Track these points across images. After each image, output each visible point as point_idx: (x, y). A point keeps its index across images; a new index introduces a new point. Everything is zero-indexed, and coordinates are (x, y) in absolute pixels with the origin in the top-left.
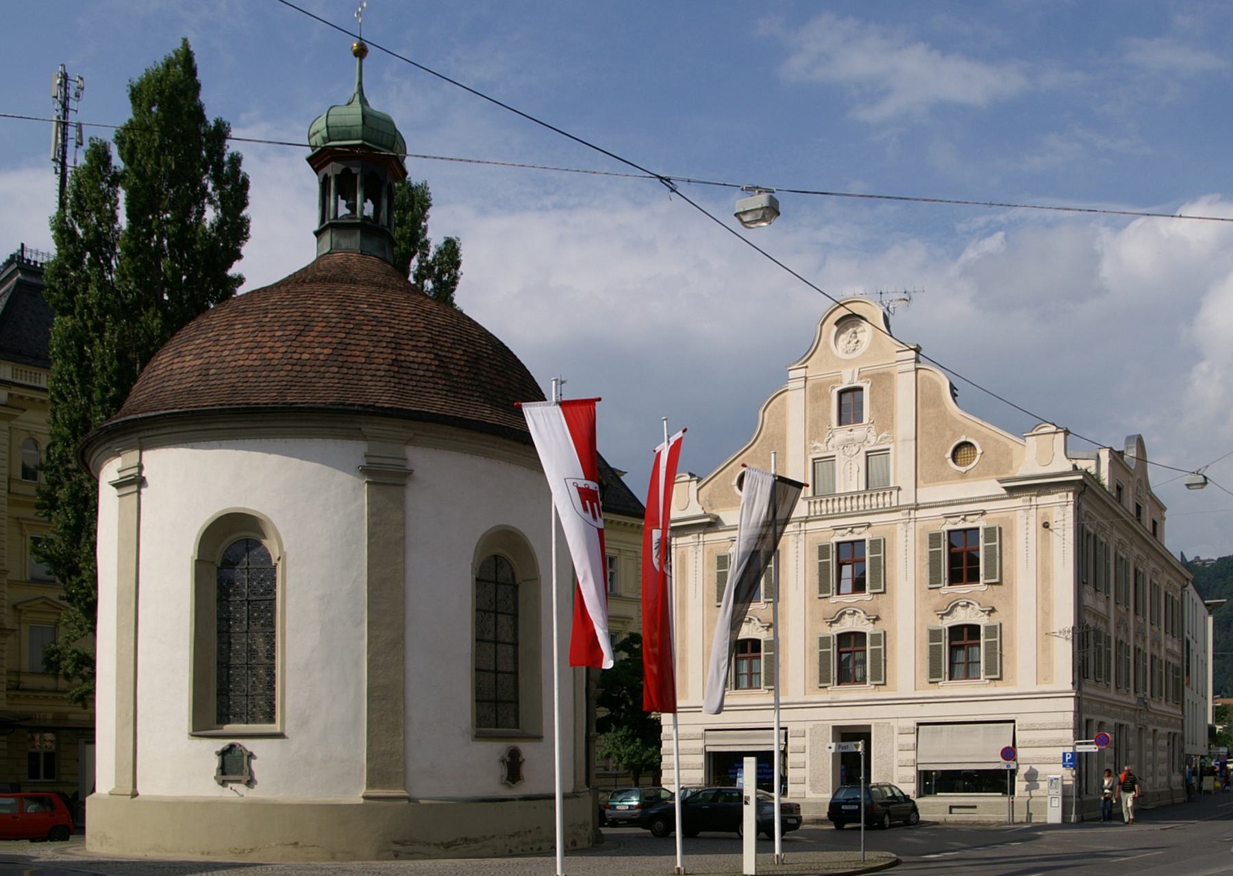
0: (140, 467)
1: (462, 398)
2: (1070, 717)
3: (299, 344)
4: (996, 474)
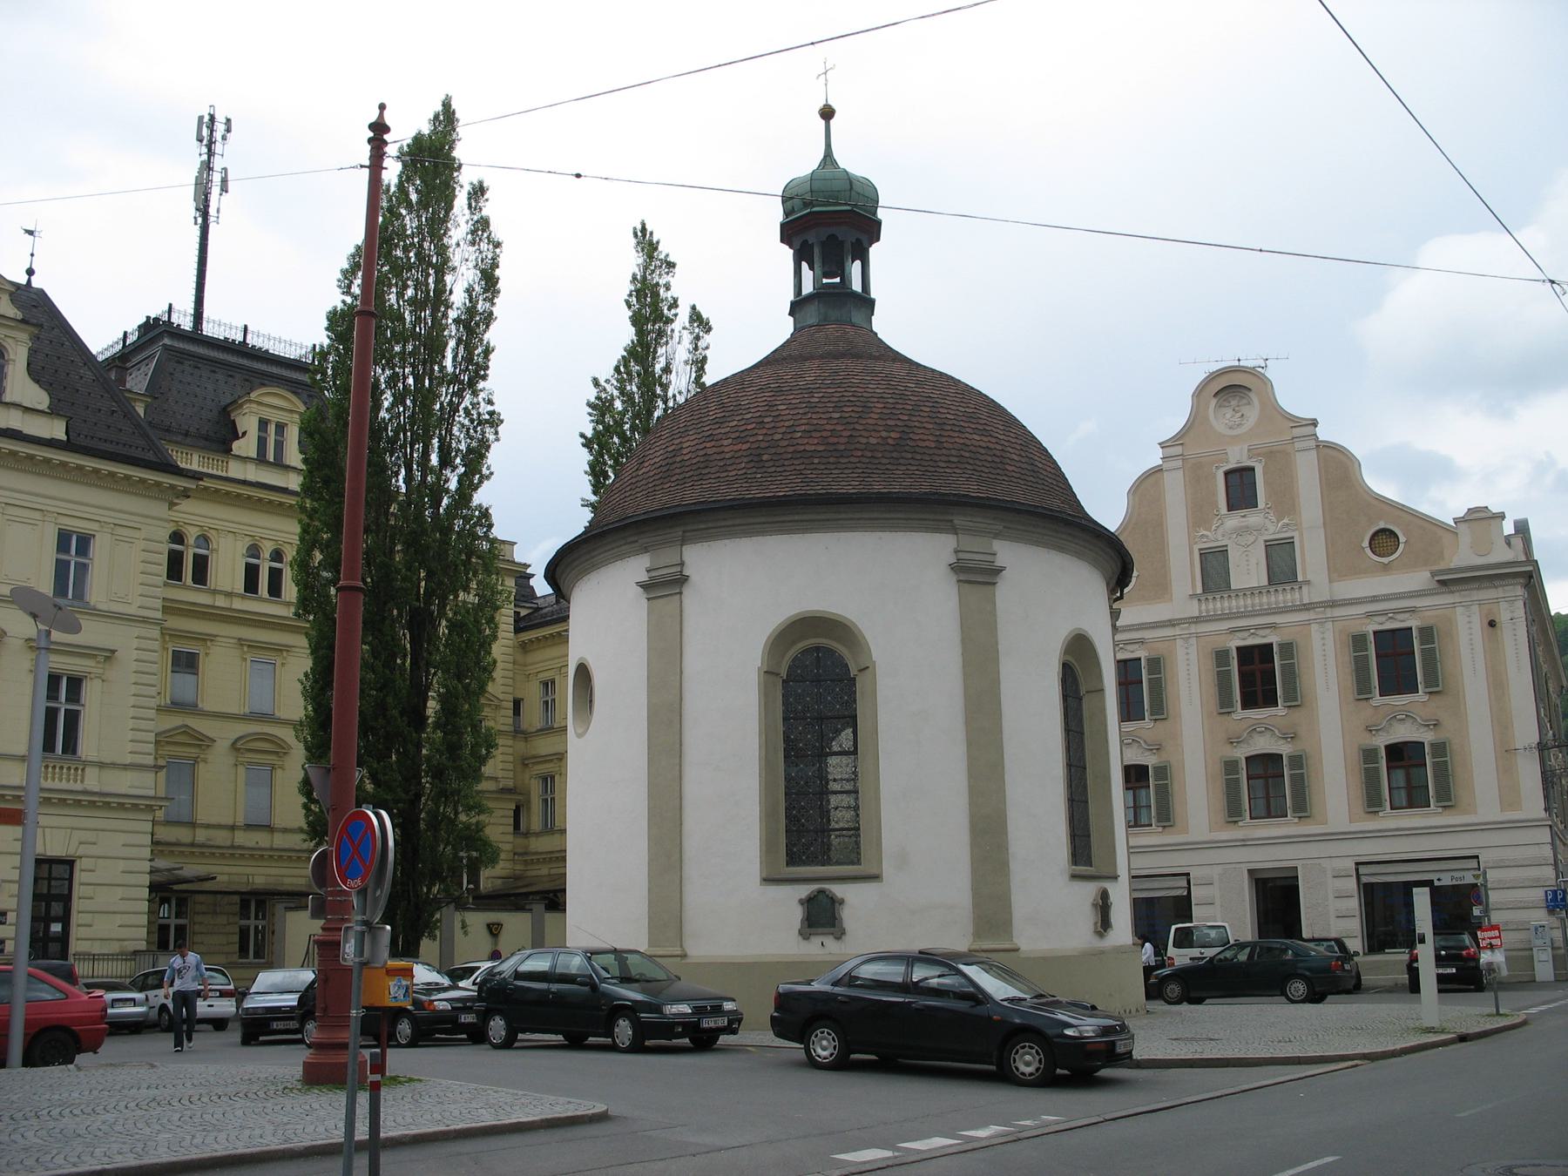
0: (682, 564)
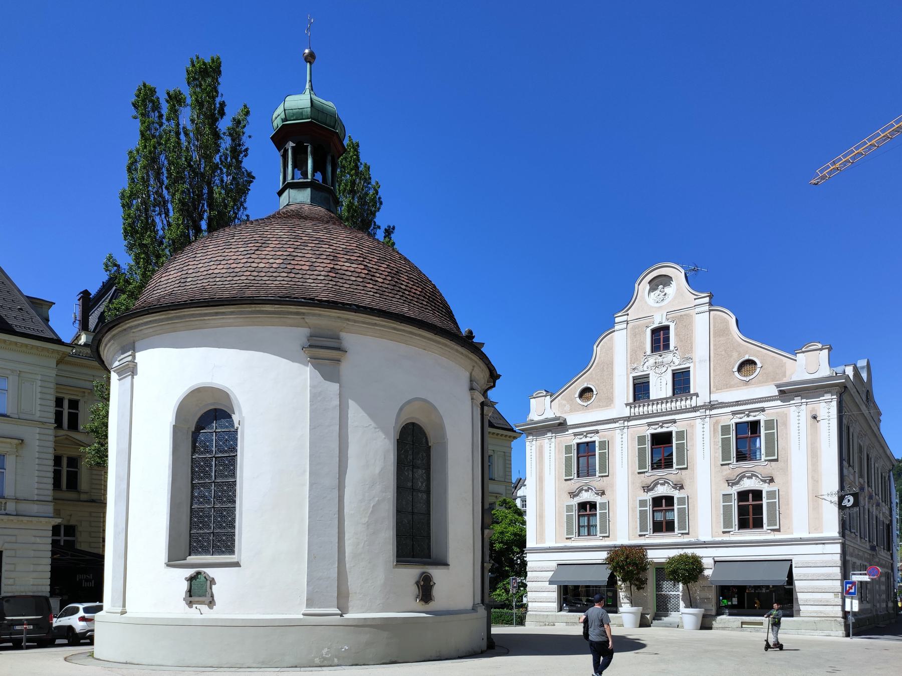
1: (385, 299)
2: (837, 558)
3: (257, 256)
4: (773, 381)
